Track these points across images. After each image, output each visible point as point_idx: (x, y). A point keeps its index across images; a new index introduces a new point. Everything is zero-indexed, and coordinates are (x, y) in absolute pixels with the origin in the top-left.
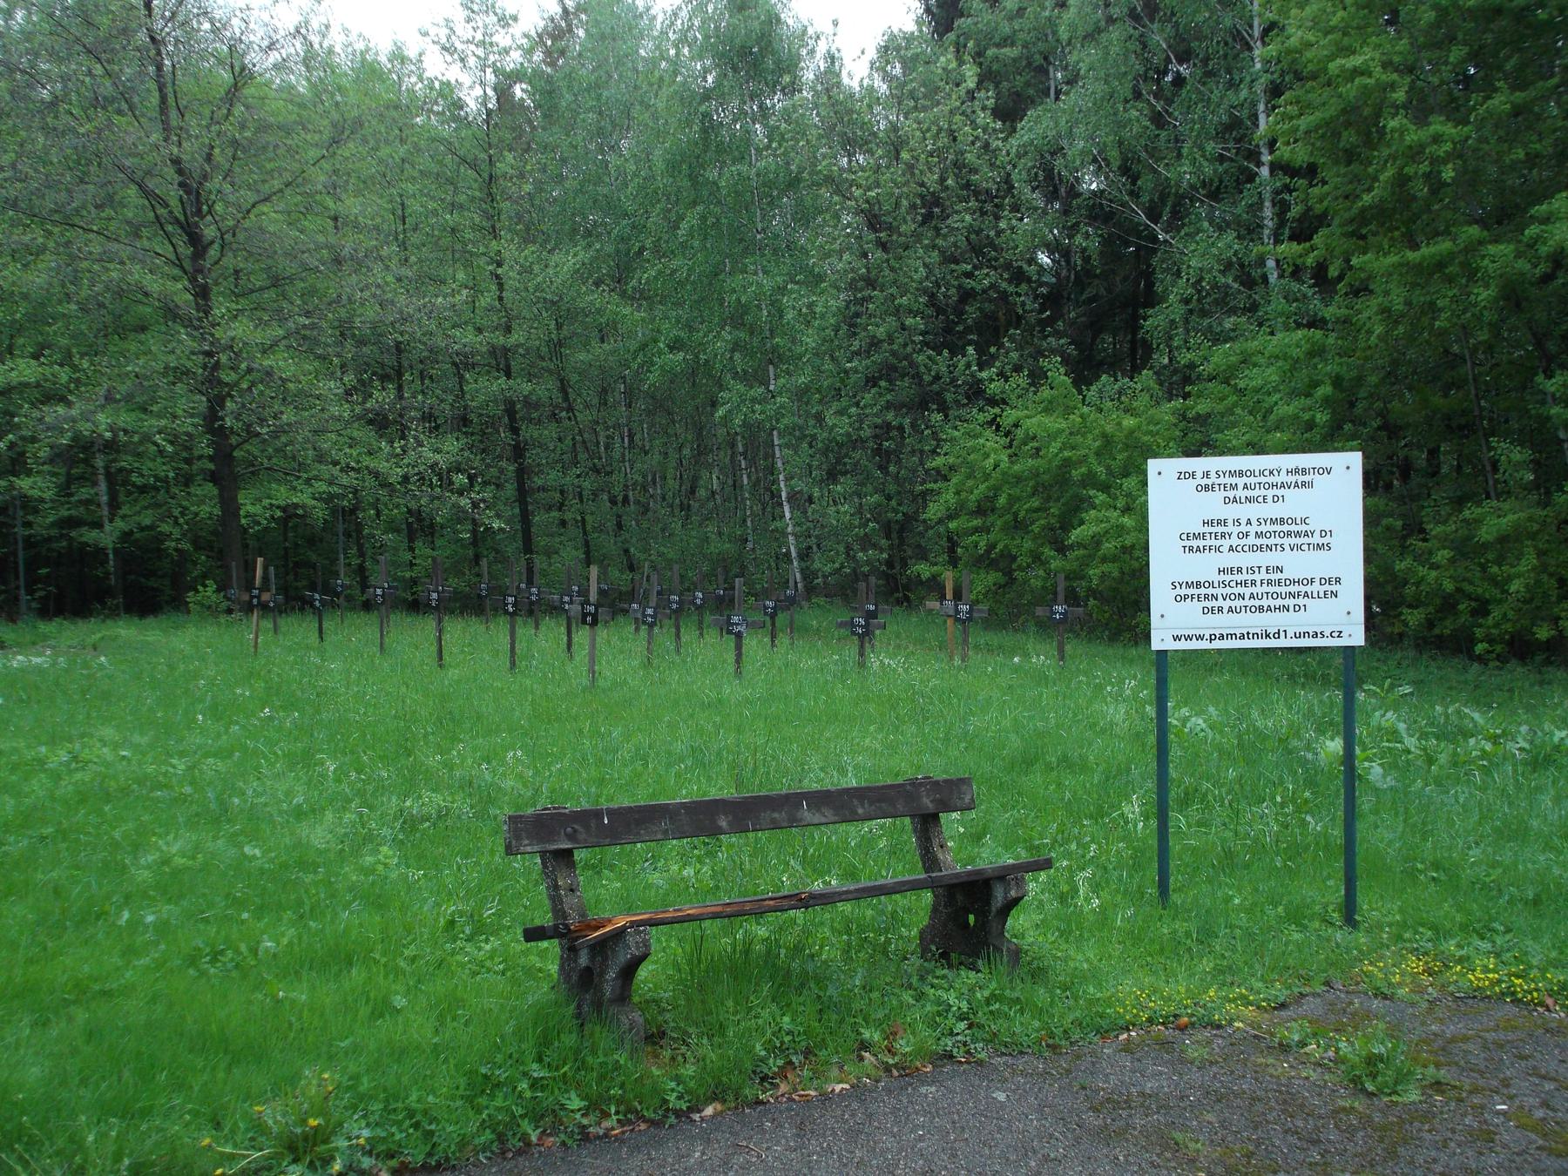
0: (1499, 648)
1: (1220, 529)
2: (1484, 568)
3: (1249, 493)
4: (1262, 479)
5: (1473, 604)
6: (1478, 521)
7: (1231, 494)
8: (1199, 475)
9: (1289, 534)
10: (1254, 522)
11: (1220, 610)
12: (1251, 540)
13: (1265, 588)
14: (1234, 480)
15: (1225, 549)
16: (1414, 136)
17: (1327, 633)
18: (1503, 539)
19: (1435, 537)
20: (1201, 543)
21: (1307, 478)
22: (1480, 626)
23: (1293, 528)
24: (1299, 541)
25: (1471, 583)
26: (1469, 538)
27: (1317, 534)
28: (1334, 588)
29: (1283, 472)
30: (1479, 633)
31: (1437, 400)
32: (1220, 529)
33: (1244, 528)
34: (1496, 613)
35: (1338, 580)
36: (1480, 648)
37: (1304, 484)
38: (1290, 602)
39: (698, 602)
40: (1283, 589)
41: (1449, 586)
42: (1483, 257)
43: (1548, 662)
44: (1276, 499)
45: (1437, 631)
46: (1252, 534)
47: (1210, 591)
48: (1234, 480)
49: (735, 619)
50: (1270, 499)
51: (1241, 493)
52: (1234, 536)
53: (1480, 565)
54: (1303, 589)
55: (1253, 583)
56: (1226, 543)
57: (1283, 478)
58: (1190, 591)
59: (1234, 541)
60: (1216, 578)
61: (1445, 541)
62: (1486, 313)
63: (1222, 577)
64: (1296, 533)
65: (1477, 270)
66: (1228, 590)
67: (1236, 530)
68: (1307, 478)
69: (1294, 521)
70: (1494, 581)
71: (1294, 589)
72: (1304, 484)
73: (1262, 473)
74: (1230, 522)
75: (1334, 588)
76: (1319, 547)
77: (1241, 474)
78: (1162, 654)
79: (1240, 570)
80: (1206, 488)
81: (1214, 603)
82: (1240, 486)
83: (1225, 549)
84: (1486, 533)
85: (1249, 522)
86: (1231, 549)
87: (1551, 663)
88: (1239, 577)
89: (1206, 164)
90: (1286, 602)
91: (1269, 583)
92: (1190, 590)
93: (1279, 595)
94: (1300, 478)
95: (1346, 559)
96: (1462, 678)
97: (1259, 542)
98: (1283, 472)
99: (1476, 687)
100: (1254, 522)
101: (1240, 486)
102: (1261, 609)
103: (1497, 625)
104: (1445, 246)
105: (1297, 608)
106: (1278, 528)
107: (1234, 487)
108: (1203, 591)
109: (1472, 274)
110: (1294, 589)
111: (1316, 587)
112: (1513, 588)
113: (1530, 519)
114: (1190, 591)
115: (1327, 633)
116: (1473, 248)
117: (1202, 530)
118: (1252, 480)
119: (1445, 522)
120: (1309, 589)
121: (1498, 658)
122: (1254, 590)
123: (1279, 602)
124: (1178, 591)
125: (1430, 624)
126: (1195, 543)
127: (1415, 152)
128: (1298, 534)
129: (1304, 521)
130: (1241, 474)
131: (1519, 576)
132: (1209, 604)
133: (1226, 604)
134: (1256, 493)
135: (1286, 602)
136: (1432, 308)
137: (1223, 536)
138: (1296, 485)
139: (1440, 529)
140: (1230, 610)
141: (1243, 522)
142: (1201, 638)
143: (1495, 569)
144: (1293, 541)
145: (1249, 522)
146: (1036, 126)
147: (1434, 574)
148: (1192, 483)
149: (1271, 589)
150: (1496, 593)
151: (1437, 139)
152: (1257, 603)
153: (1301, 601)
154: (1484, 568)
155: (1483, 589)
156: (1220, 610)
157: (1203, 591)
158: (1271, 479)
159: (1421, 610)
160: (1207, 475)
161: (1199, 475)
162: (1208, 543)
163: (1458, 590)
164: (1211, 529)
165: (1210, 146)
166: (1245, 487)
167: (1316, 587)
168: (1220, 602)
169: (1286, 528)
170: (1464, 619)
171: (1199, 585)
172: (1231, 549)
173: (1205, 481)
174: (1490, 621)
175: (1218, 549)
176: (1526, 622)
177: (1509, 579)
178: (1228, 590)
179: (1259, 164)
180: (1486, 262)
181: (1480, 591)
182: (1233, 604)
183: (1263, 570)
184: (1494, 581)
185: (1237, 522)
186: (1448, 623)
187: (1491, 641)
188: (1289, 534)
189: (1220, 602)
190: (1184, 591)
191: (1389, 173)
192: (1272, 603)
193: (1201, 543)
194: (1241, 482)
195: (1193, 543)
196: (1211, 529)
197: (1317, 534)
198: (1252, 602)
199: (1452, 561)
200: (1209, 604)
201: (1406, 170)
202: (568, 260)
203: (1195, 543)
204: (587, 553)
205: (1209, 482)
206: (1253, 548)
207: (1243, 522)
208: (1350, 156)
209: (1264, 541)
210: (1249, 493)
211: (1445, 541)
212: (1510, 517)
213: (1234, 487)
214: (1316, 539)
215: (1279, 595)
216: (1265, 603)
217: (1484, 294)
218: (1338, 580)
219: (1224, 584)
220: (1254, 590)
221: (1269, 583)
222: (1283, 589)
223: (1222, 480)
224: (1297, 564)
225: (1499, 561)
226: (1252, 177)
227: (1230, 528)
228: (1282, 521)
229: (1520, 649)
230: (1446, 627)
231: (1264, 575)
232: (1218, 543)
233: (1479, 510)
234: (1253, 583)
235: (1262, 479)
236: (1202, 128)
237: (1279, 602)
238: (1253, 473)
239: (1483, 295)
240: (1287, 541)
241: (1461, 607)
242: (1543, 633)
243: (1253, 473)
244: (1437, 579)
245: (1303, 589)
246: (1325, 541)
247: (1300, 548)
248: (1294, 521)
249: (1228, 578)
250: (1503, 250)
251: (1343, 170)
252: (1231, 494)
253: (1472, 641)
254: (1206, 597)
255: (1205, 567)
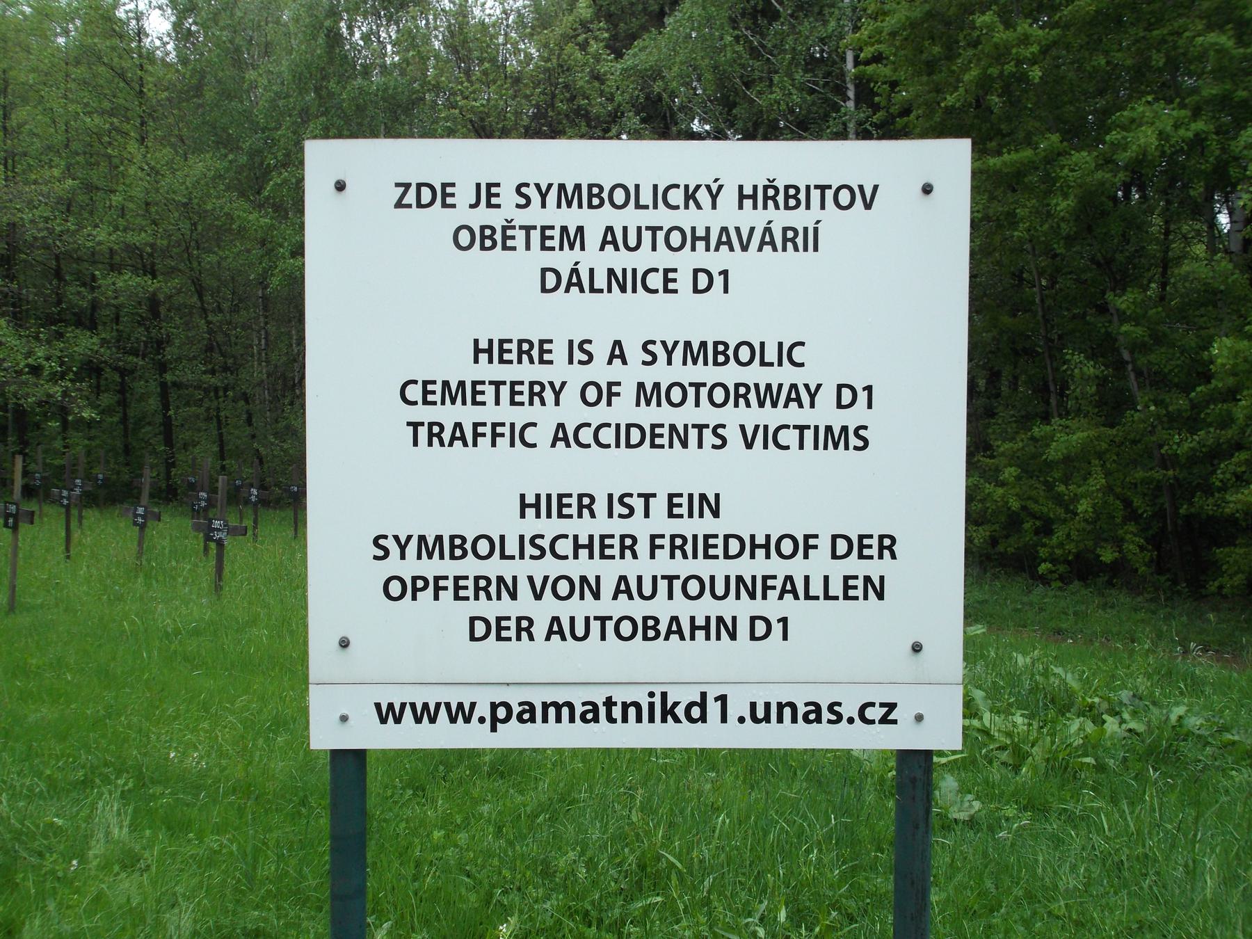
0: (1062, 568)
1: (527, 372)
2: (1050, 487)
3: (620, 260)
4: (663, 217)
5: (1038, 523)
6: (1049, 439)
7: (563, 260)
8: (464, 195)
9: (740, 394)
10: (634, 353)
11: (525, 627)
12: (624, 410)
13: (665, 564)
14: (572, 217)
15: (542, 435)
16: (1001, 35)
17: (849, 710)
18: (1067, 460)
19: (1003, 454)
20: (467, 415)
21: (800, 219)
22: (1044, 545)
23: (755, 375)
24: (771, 416)
25: (1036, 502)
26: (1034, 457)
27: (826, 397)
28: (873, 568)
29: (728, 197)
30: (1043, 552)
31: (1006, 320)
32: (527, 372)
33: (601, 372)
34: (1060, 533)
35: (887, 545)
36: (1043, 568)
37: (790, 238)
38: (740, 609)
39: (253, 499)
40: (720, 569)
41: (1015, 504)
42: (1062, 168)
43: (1110, 584)
44: (703, 282)
45: (1000, 548)
46: (628, 392)
47: (494, 568)
48: (572, 217)
49: (217, 524)
50: (684, 281)
51: (596, 259)
52: (571, 395)
53: (1046, 483)
54: (778, 567)
55: (628, 545)
56: (546, 417)
57: (728, 214)
58: (431, 568)
59: (572, 412)
60: (514, 527)
61: (1013, 459)
62: (1063, 225)
63: (532, 525)
64: (762, 391)
65: (1055, 180)
66: (550, 567)
67: (576, 376)
68: (800, 219)
69: (758, 354)
70: (1058, 499)
71: (748, 567)
72: (790, 238)
73: (661, 196)
74: (559, 352)
75: (873, 568)
76: (833, 438)
77: (595, 196)
78: (350, 763)
79: (586, 504)
80: (486, 238)
81: (505, 607)
82: (593, 237)
83: (542, 435)
84: (1055, 451)
85: (617, 353)
86: (560, 435)
87: (1114, 586)
88: (584, 527)
89: (794, 91)
90: (727, 608)
91: (677, 545)
92: (430, 563)
93: (707, 586)
94: (781, 219)
95: (915, 473)
96: (1025, 599)
97: (648, 415)
98: (728, 197)
99: (1041, 610)
100: (634, 353)
101: (593, 237)
102: (649, 629)
103: (1061, 545)
104: (1027, 153)
105: (760, 629)
106: (707, 374)
107: (574, 238)
108: (470, 567)
109: (1049, 181)
110: (748, 567)
111: (818, 565)
112: (1080, 509)
113: (1098, 438)
114: (431, 568)
115: (849, 710)
116: (1052, 158)
117: (471, 372)
118: (631, 218)
119: (1012, 439)
120: (797, 568)
121: (1061, 578)
122: (629, 567)
123: (707, 608)
124: (393, 565)
125: (994, 542)
126: (448, 414)
127: (1001, 53)
128: (768, 396)
129: (787, 354)
130: (595, 196)
131: (1084, 496)
132: (490, 609)
133: (543, 611)
134: (642, 259)
135: (727, 608)
136: (1011, 219)
137: (536, 392)
138: (767, 240)
139: (1008, 445)
140: (555, 628)
141: (601, 350)
142: (461, 713)
143: (1062, 488)
144: (753, 416)
145: (617, 353)
146: (641, 55)
147: (1000, 491)
148: (441, 221)
149: (682, 567)
150: (1060, 511)
151: (1025, 40)
152: (638, 609)
153: (772, 607)
154: (1050, 487)
155: (1047, 508)
156: (525, 627)
157: (470, 567)
158: (688, 218)
159: (986, 527)
160: (487, 194)
161: (464, 195)
162: (489, 414)
163: (1024, 508)
164: (498, 371)
165: (799, 76)
166: (609, 239)
167: (818, 565)
168: (525, 604)
169: (731, 374)
170: (1029, 538)
171: (458, 547)
172: (560, 435)
173: (482, 217)
174: (1055, 540)
175: (519, 436)
176: (1090, 543)
177: (1076, 499)
178: (550, 567)
179: (846, 99)
180: (1066, 171)
181: (1045, 510)
182: (564, 610)
183: (659, 506)
184: (1058, 499)
185: (581, 351)
186: (1011, 540)
187: (1054, 561)
188: (740, 394)
189: (525, 604)
190: (411, 567)
191: (973, 74)
192: (684, 609)
193: (467, 415)
194: (594, 222)
195: (443, 413)
196: (498, 371)
197: (826, 397)
198: (623, 606)
199: (1018, 478)
200: (490, 609)
201: (990, 71)
202: (201, 166)
203: (448, 414)
204: (222, 446)
205: (495, 219)
206: (627, 436)
207: (601, 350)
208: (931, 67)
209: (664, 415)
210: (620, 260)
211: (1013, 459)
212: (1080, 435)
213: (574, 238)
214: (825, 413)
215: (707, 586)
216: (662, 608)
217: (1064, 204)
218: (887, 545)
219: (538, 547)
220: (629, 567)
221: (677, 545)
222: (720, 569)
223: (535, 215)
224: (765, 490)
225: (1066, 480)
226: (836, 108)
227: (558, 370)
228: (720, 353)
229: (1082, 569)
230: (1010, 546)
231: (660, 522)
232: (519, 416)
233: (1048, 428)
234: (628, 545)
235: (663, 217)
236: (793, 58)
237: (707, 608)
238: (632, 197)
239: (1063, 205)
240: (734, 417)
241: (1027, 526)
242: (1108, 556)
243: (632, 197)
244: (1003, 496)
245: (778, 567)
246: (851, 418)
247: (772, 438)
248: (758, 354)
249: (550, 527)
250: (1083, 157)
251: (925, 78)
252: (563, 260)
253: (1035, 560)
254: (482, 586)
255: (478, 491)
